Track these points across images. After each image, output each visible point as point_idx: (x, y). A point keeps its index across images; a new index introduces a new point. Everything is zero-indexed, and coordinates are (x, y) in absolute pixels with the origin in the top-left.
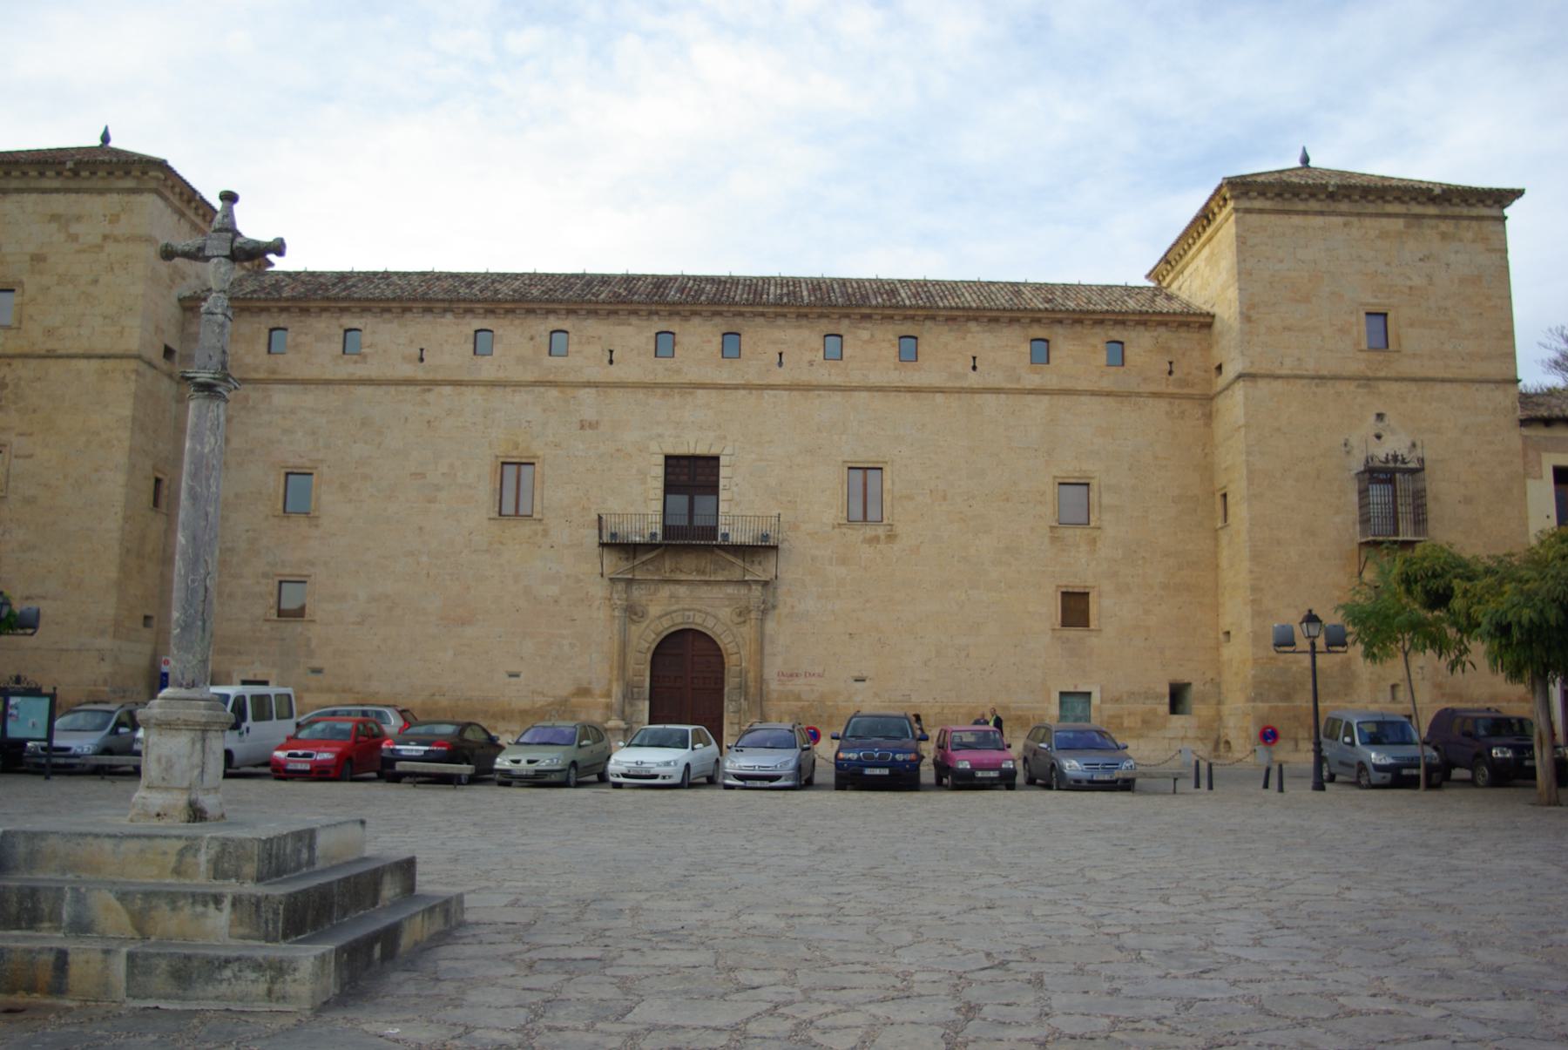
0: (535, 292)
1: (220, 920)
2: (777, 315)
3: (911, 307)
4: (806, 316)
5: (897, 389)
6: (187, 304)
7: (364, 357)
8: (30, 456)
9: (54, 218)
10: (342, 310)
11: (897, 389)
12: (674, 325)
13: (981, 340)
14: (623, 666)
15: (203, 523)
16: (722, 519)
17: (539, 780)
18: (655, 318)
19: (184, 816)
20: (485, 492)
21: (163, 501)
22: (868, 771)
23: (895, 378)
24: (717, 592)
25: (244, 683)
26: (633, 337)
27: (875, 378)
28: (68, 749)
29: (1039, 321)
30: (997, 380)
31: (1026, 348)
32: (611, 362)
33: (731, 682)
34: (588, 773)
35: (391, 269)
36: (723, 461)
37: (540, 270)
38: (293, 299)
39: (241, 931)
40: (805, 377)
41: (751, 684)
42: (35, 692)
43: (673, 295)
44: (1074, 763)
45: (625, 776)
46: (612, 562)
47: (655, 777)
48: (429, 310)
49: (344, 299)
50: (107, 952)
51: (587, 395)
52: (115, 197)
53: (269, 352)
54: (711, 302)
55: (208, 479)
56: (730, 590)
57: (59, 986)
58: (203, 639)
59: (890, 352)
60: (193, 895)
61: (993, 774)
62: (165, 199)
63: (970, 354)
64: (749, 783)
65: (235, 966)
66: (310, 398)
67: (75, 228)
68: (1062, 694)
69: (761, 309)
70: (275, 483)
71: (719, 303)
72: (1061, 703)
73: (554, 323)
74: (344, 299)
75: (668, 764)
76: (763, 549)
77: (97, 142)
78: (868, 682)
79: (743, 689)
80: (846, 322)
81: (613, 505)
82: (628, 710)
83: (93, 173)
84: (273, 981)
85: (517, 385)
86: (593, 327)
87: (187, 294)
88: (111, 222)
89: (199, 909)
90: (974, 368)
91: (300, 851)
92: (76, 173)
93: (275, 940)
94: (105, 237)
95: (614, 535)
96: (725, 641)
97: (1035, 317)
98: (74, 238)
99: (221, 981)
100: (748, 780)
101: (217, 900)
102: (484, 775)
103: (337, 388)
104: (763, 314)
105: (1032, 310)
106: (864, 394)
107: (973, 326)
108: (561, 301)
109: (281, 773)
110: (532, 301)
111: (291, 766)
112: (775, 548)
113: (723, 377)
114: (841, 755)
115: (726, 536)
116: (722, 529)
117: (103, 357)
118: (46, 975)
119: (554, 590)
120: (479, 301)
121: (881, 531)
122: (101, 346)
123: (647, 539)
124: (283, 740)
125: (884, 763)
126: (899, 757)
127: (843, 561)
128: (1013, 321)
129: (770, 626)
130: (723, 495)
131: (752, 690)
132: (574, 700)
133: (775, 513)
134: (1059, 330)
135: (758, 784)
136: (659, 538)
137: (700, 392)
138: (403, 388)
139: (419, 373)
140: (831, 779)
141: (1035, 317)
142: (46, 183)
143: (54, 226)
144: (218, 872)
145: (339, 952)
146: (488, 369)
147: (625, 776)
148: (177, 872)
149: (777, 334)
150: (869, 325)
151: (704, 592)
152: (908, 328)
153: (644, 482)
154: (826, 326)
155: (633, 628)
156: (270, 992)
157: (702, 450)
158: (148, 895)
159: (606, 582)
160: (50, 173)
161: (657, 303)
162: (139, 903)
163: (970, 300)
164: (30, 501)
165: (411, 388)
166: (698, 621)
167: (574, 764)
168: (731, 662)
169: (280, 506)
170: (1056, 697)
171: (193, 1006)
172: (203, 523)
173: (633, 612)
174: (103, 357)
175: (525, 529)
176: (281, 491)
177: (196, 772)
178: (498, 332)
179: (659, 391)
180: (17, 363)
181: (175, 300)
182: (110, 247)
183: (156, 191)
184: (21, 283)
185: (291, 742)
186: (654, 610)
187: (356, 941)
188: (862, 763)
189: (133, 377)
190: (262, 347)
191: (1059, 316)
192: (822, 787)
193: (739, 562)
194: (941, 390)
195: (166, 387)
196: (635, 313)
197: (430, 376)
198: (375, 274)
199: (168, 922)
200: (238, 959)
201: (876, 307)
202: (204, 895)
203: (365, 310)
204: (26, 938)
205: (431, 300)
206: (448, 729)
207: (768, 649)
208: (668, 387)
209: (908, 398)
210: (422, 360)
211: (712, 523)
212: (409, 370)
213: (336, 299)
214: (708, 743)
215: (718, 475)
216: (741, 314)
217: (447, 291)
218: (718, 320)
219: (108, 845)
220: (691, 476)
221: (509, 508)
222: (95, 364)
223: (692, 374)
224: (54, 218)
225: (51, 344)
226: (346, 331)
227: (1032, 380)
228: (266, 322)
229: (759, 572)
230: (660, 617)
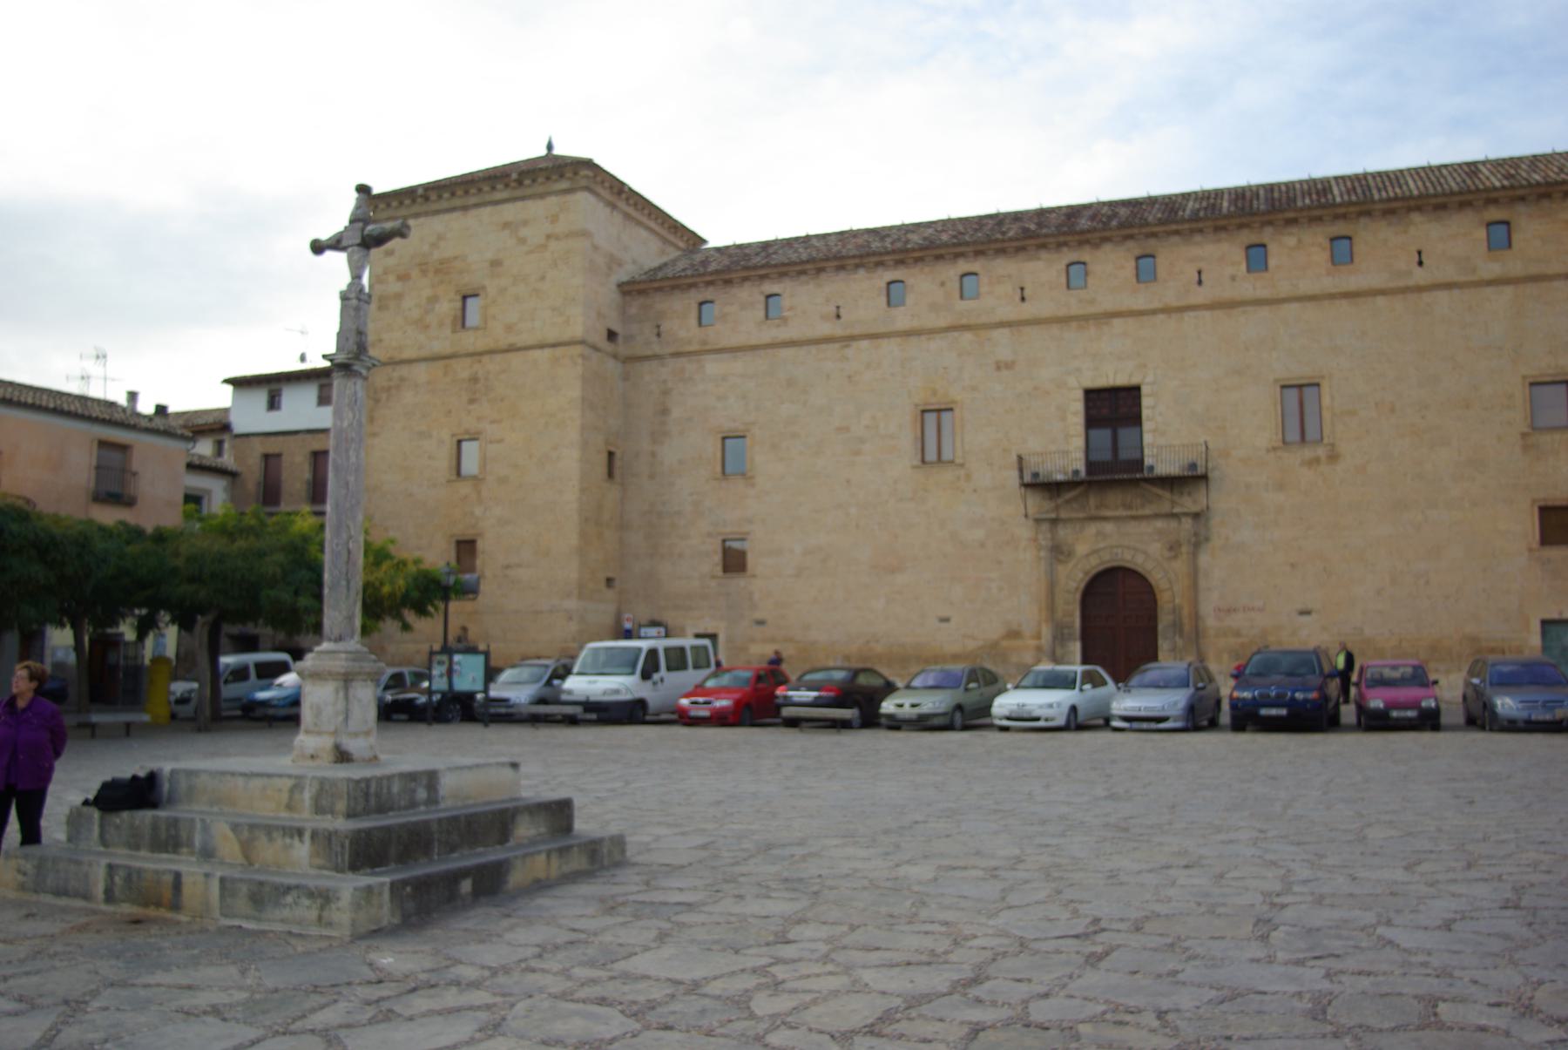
0: (945, 237)
1: (302, 850)
2: (1192, 231)
3: (1340, 205)
4: (1224, 228)
5: (1332, 297)
6: (626, 288)
7: (784, 320)
8: (501, 441)
9: (506, 225)
10: (763, 277)
11: (1332, 297)
12: (1085, 255)
13: (1425, 231)
14: (1051, 607)
15: (344, 492)
16: (1146, 451)
17: (923, 724)
18: (1065, 249)
19: (331, 758)
20: (906, 441)
21: (617, 472)
22: (1264, 712)
23: (1329, 284)
24: (1146, 528)
25: (698, 636)
26: (1043, 271)
27: (1306, 286)
28: (506, 700)
29: (1495, 201)
30: (1450, 273)
31: (1482, 233)
32: (1023, 299)
33: (1164, 621)
34: (970, 717)
35: (812, 232)
36: (1145, 390)
37: (954, 215)
38: (717, 272)
39: (320, 861)
40: (1229, 293)
41: (1186, 621)
42: (472, 650)
43: (1084, 223)
44: (1508, 701)
45: (1008, 718)
46: (1036, 503)
47: (1038, 719)
48: (841, 268)
49: (763, 267)
50: (207, 875)
51: (1002, 335)
52: (553, 200)
53: (700, 324)
54: (1121, 226)
55: (347, 451)
56: (1159, 524)
57: (176, 906)
58: (347, 597)
59: (1320, 256)
60: (284, 828)
61: (1411, 714)
62: (597, 194)
63: (1414, 249)
64: (1136, 725)
65: (295, 893)
66: (738, 365)
67: (524, 232)
68: (1544, 623)
69: (1174, 227)
70: (712, 447)
71: (1131, 226)
72: (1544, 634)
73: (963, 266)
74: (763, 267)
75: (1050, 706)
76: (1192, 479)
77: (543, 152)
78: (1314, 616)
79: (1177, 627)
80: (1269, 230)
81: (1032, 446)
82: (1059, 652)
83: (534, 181)
84: (322, 908)
85: (932, 332)
86: (1003, 266)
87: (625, 278)
88: (552, 222)
89: (288, 841)
90: (1420, 263)
91: (414, 791)
92: (520, 182)
93: (342, 871)
94: (548, 237)
95: (1036, 475)
96: (1157, 578)
97: (1491, 198)
98: (522, 241)
99: (285, 906)
100: (1137, 722)
101: (300, 832)
102: (871, 719)
103: (762, 352)
104: (1177, 232)
105: (1486, 190)
106: (1295, 306)
107: (1416, 217)
108: (967, 244)
109: (685, 719)
110: (939, 247)
111: (693, 713)
112: (1204, 478)
113: (1140, 301)
114: (1236, 694)
115: (1151, 468)
116: (1148, 461)
117: (554, 345)
118: (167, 894)
119: (979, 534)
120: (888, 253)
121: (1321, 452)
122: (552, 335)
123: (1069, 477)
124: (690, 688)
125: (1304, 700)
126: (1299, 696)
127: (1281, 487)
128: (1463, 205)
129: (1204, 559)
130: (1147, 425)
131: (1187, 628)
132: (1005, 643)
133: (1202, 440)
134: (1521, 208)
135: (1145, 725)
136: (1083, 474)
137: (1117, 322)
138: (824, 346)
139: (836, 329)
140: (1460, 719)
141: (1491, 198)
142: (498, 196)
143: (507, 232)
144: (319, 809)
145: (392, 884)
146: (902, 319)
147: (1008, 718)
148: (290, 807)
149: (1195, 251)
150: (1294, 230)
151: (1133, 528)
152: (1340, 228)
153: (1063, 419)
154: (1248, 237)
155: (1060, 568)
156: (320, 918)
157: (1121, 380)
158: (252, 827)
159: (1031, 523)
160: (500, 186)
161: (1064, 234)
162: (246, 834)
163: (1413, 187)
164: (503, 480)
165: (831, 346)
166: (1128, 558)
167: (959, 707)
168: (1164, 599)
169: (719, 469)
170: (1536, 627)
171: (264, 926)
172: (344, 492)
173: (1058, 552)
174: (554, 345)
175: (948, 475)
176: (719, 455)
177: (341, 718)
178: (910, 281)
179: (1074, 324)
180: (486, 359)
181: (614, 287)
182: (553, 245)
183: (587, 189)
184: (484, 288)
185: (699, 690)
186: (1081, 549)
187: (429, 876)
188: (1256, 703)
189: (580, 361)
190: (693, 321)
191: (1520, 192)
192: (1453, 728)
193: (1167, 495)
194: (1383, 292)
195: (612, 367)
196: (1043, 246)
197: (848, 332)
198: (797, 239)
199: (267, 851)
200: (297, 887)
201: (1302, 209)
202: (291, 828)
203: (783, 275)
204: (171, 861)
205: (843, 258)
206: (839, 675)
207: (1202, 583)
208: (1083, 319)
209: (1344, 304)
210: (838, 317)
211: (1136, 455)
212: (826, 329)
213: (755, 268)
214: (1104, 683)
215: (1139, 405)
216: (1154, 235)
217: (858, 247)
218: (1130, 244)
219: (240, 781)
220: (1112, 408)
221: (931, 455)
222: (547, 352)
223: (1107, 303)
224: (506, 225)
225: (513, 339)
226: (768, 297)
227: (1493, 269)
228: (695, 296)
229: (1188, 503)
230: (1087, 556)
